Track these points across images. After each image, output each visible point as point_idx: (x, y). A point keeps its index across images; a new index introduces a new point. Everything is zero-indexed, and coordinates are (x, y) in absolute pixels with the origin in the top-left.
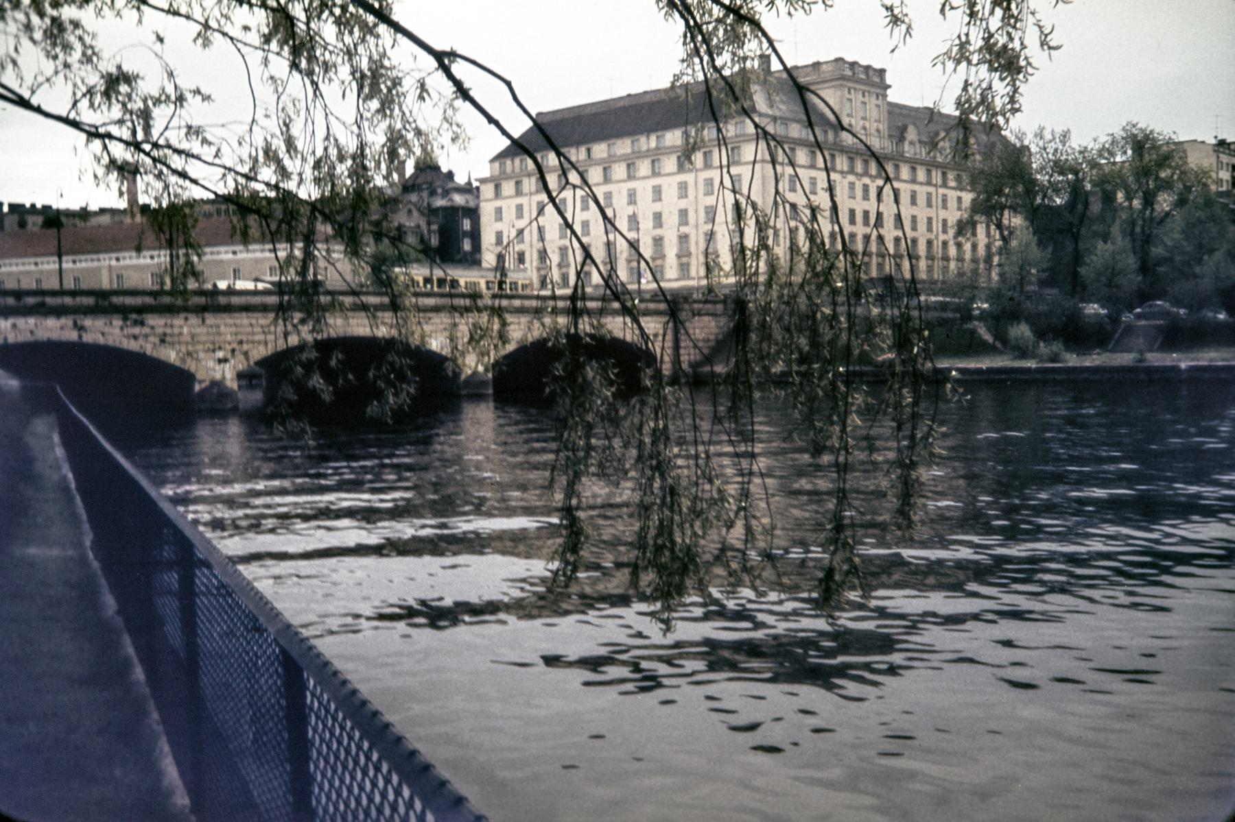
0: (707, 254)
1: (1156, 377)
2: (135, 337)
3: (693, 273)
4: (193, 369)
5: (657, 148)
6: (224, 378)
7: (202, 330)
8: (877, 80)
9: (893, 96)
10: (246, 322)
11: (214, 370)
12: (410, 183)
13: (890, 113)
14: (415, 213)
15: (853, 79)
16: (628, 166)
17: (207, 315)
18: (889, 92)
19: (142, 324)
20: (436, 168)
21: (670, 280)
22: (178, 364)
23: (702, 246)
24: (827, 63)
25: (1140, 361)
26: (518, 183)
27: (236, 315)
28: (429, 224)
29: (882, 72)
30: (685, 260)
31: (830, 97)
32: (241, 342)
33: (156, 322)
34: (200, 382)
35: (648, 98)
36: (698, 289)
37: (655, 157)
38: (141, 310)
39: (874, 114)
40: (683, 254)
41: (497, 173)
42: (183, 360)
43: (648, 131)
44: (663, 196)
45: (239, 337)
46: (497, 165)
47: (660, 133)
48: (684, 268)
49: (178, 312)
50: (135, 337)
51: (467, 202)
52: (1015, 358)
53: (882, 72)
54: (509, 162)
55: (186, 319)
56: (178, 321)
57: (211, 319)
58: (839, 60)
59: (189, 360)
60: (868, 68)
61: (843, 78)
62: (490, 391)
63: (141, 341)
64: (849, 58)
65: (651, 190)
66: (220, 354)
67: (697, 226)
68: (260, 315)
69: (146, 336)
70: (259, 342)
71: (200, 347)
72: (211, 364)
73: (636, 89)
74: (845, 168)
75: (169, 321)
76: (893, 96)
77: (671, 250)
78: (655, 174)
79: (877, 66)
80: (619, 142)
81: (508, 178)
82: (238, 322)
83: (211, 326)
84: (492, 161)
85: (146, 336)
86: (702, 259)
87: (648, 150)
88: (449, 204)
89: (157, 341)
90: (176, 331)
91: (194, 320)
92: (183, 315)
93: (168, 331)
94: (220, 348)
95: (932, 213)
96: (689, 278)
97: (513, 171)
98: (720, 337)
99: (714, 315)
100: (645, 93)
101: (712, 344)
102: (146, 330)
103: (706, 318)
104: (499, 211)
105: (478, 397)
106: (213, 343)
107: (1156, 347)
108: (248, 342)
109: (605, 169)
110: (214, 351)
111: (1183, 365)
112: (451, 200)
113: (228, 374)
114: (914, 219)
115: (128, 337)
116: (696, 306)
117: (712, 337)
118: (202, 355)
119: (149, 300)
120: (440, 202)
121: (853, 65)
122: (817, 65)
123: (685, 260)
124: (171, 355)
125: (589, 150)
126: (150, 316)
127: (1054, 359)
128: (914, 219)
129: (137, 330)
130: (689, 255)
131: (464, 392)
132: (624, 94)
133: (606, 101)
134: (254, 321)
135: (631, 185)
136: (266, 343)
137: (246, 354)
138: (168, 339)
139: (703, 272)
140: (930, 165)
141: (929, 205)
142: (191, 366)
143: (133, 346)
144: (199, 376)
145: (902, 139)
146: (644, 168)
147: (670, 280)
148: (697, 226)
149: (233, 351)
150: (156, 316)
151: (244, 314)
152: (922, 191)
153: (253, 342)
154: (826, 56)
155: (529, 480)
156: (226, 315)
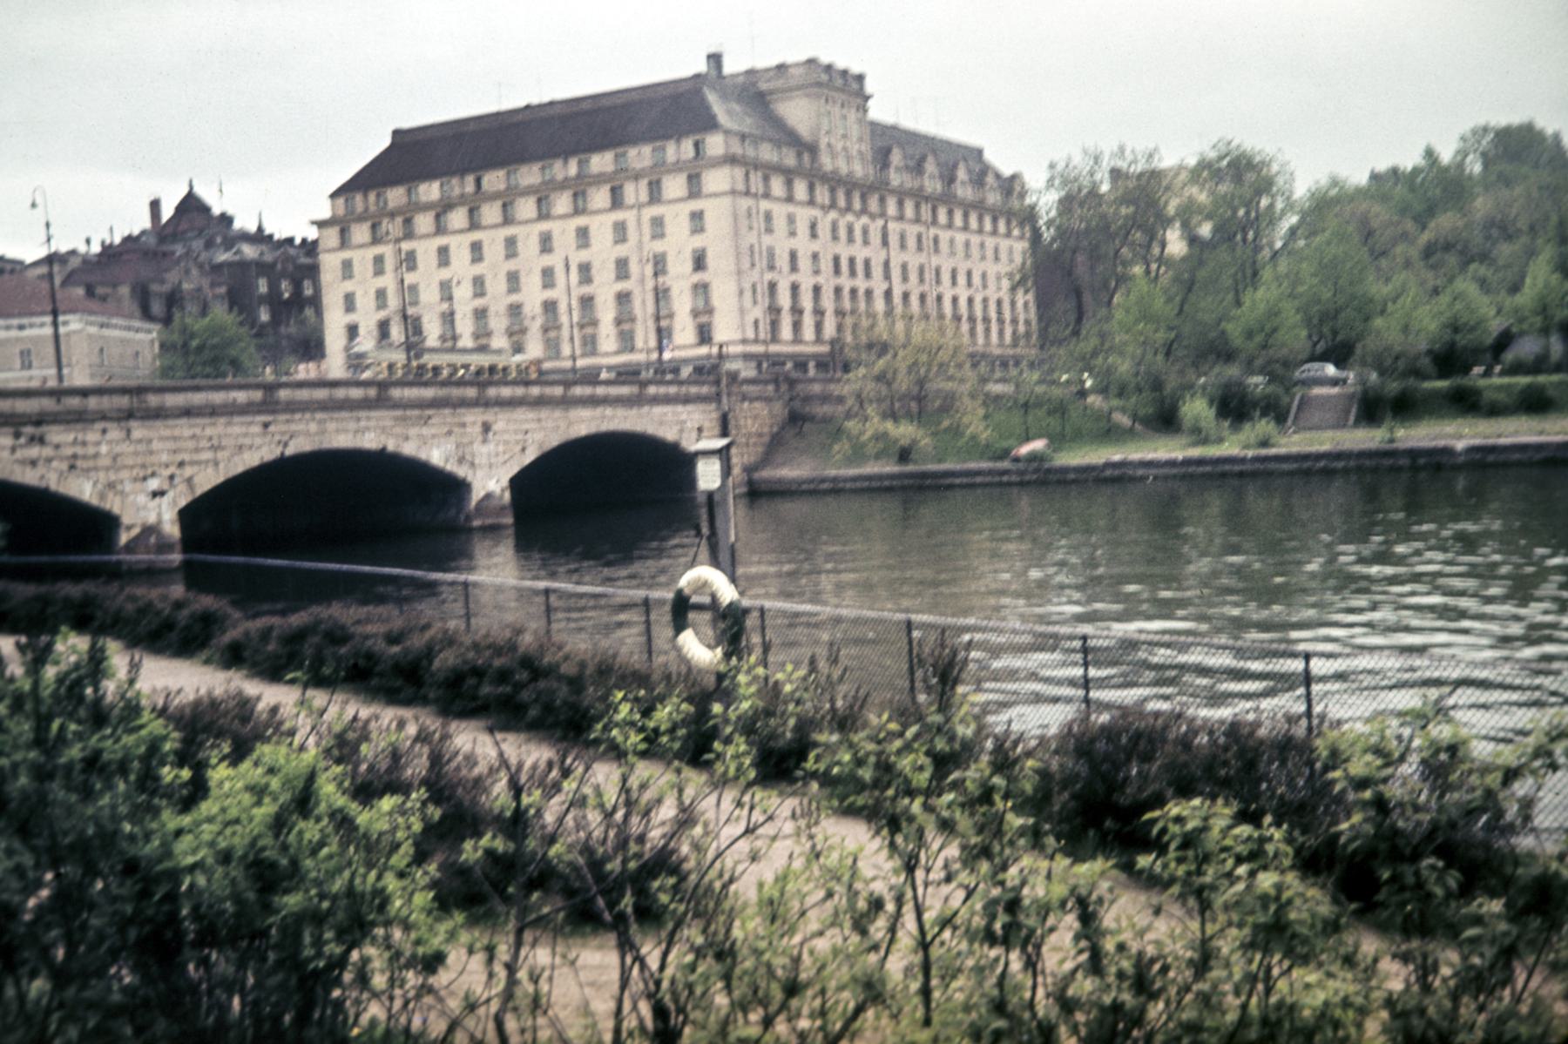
0: (658, 318)
1: (1422, 461)
2: (33, 463)
3: (639, 343)
4: (116, 510)
5: (579, 176)
6: (160, 522)
7: (126, 448)
8: (855, 86)
9: (879, 111)
10: (187, 432)
11: (145, 508)
12: (169, 230)
13: (873, 133)
14: (195, 272)
15: (829, 85)
16: (539, 201)
17: (133, 424)
18: (870, 103)
19: (41, 441)
20: (205, 209)
21: (607, 354)
22: (95, 502)
23: (651, 308)
24: (797, 65)
25: (1392, 441)
26: (408, 222)
27: (171, 422)
28: (213, 285)
29: (860, 78)
30: (626, 327)
31: (798, 113)
32: (181, 464)
33: (58, 435)
34: (129, 528)
35: (557, 110)
36: (648, 365)
37: (579, 189)
38: (40, 420)
39: (855, 131)
40: (624, 320)
41: (341, 211)
42: (102, 496)
43: (566, 155)
44: (593, 241)
45: (179, 458)
46: (341, 201)
47: (583, 156)
48: (626, 341)
49: (93, 421)
50: (33, 463)
51: (262, 254)
52: (1195, 444)
53: (860, 78)
54: (359, 198)
55: (104, 431)
56: (92, 436)
57: (139, 431)
58: (811, 62)
59: (111, 495)
60: (845, 73)
61: (819, 84)
62: (509, 520)
63: (40, 470)
64: (825, 59)
65: (573, 234)
66: (154, 484)
67: (642, 281)
68: (206, 421)
69: (49, 460)
70: (207, 462)
71: (125, 474)
72: (142, 499)
73: (535, 100)
74: (827, 202)
75: (80, 437)
76: (879, 111)
77: (606, 314)
78: (543, 216)
79: (855, 69)
80: (524, 169)
81: (361, 219)
82: (177, 432)
83: (140, 441)
84: (334, 196)
85: (49, 460)
86: (651, 324)
87: (566, 179)
88: (237, 258)
89: (64, 466)
90: (91, 450)
91: (115, 433)
92: (99, 426)
93: (79, 450)
94: (153, 475)
95: (922, 258)
96: (632, 349)
97: (366, 209)
98: (775, 429)
99: (768, 400)
100: (551, 103)
101: (766, 439)
102: (47, 451)
103: (757, 405)
104: (347, 266)
105: (492, 530)
106: (144, 466)
107: (1352, 418)
108: (193, 463)
109: (504, 206)
110: (145, 479)
111: (1460, 445)
112: (238, 252)
113: (165, 515)
114: (904, 267)
115: (23, 462)
116: (745, 388)
117: (766, 430)
118: (128, 487)
119: (47, 404)
120: (223, 257)
121: (829, 68)
122: (781, 68)
123: (626, 327)
124: (84, 490)
125: (478, 182)
126: (54, 428)
127: (1265, 443)
128: (904, 267)
129: (34, 451)
130: (633, 320)
131: (476, 523)
132: (521, 103)
133: (498, 115)
134: (198, 431)
135: (544, 226)
136: (216, 464)
137: (189, 481)
138: (79, 463)
139: (653, 343)
140: (919, 196)
141: (920, 248)
142: (113, 505)
143: (29, 477)
144: (126, 520)
145: (885, 165)
146: (562, 203)
147: (607, 354)
148: (642, 281)
149: (172, 477)
150: (62, 428)
151: (183, 421)
152: (912, 230)
153: (198, 463)
154: (794, 56)
155: (432, 639)
156: (158, 423)
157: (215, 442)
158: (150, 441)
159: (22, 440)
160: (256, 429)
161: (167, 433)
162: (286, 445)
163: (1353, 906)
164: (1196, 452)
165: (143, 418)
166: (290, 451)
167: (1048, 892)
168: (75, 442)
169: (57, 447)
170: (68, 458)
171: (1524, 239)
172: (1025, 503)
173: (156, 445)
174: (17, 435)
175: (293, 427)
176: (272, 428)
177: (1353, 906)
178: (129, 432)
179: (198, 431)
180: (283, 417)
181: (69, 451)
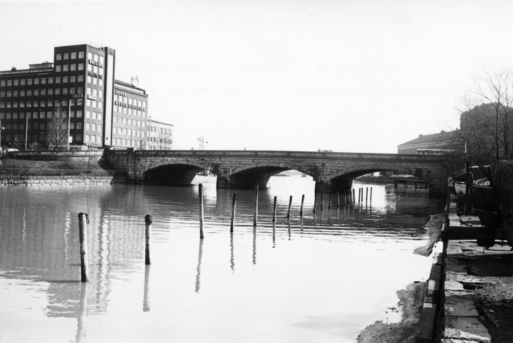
55: (216, 159)
69: (205, 163)
82: (231, 160)
134: (236, 160)
157: (240, 163)
158: (225, 161)
159: (200, 160)
160: (251, 161)
161: (229, 160)
162: (258, 165)
163: (122, 172)
164: (466, 226)
165: (224, 157)
166: (259, 166)
167: (68, 228)
168: (210, 161)
169: (206, 161)
170: (208, 163)
171: (123, 239)
172: (455, 221)
173: (226, 162)
174: (199, 159)
175: (261, 161)
176: (255, 161)
177: (122, 172)
178: (221, 159)
179: (236, 160)
180: (258, 158)
181: (208, 162)
